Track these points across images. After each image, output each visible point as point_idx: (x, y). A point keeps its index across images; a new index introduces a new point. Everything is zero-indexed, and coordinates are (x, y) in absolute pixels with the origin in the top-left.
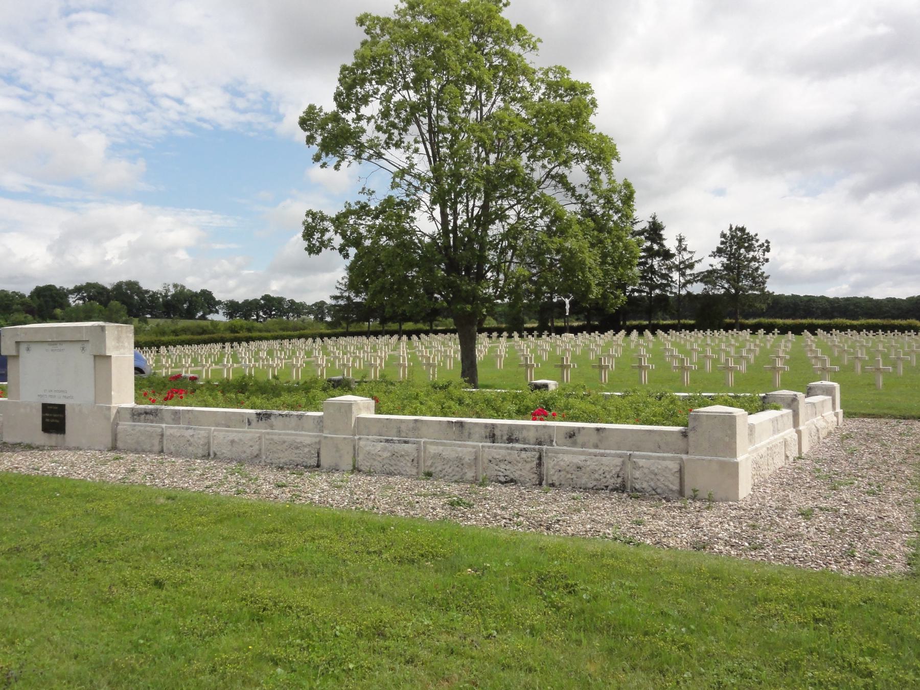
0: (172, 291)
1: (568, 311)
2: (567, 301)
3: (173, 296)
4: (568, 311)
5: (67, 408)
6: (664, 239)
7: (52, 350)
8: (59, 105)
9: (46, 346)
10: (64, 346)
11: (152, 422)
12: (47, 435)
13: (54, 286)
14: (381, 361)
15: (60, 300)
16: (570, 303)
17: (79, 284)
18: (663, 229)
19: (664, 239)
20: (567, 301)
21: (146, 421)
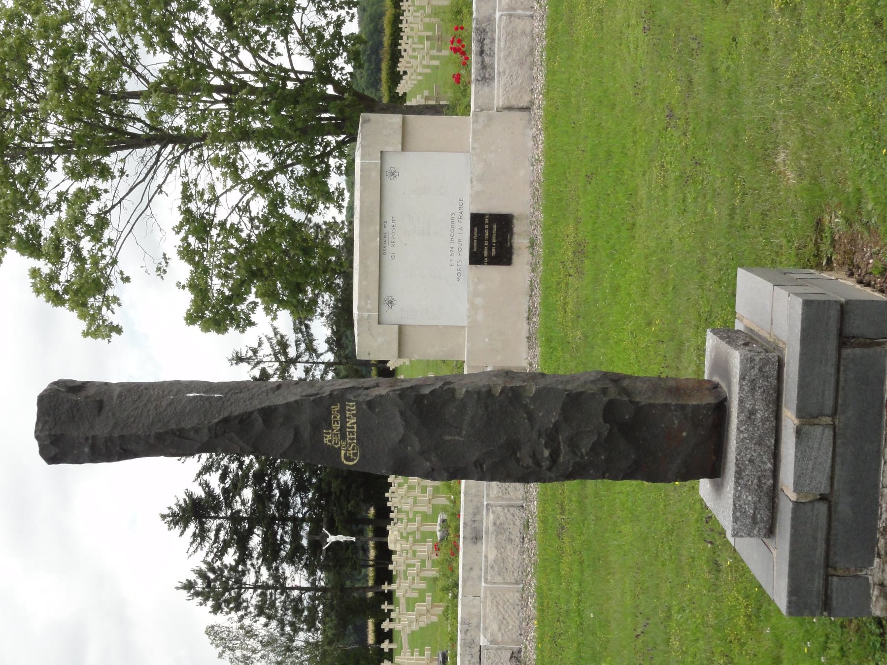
1: (349, 538)
2: (332, 539)
4: (349, 538)
5: (475, 212)
7: (393, 246)
9: (387, 258)
10: (388, 218)
11: (493, 40)
12: (515, 258)
16: (334, 533)
20: (332, 539)
21: (492, 56)
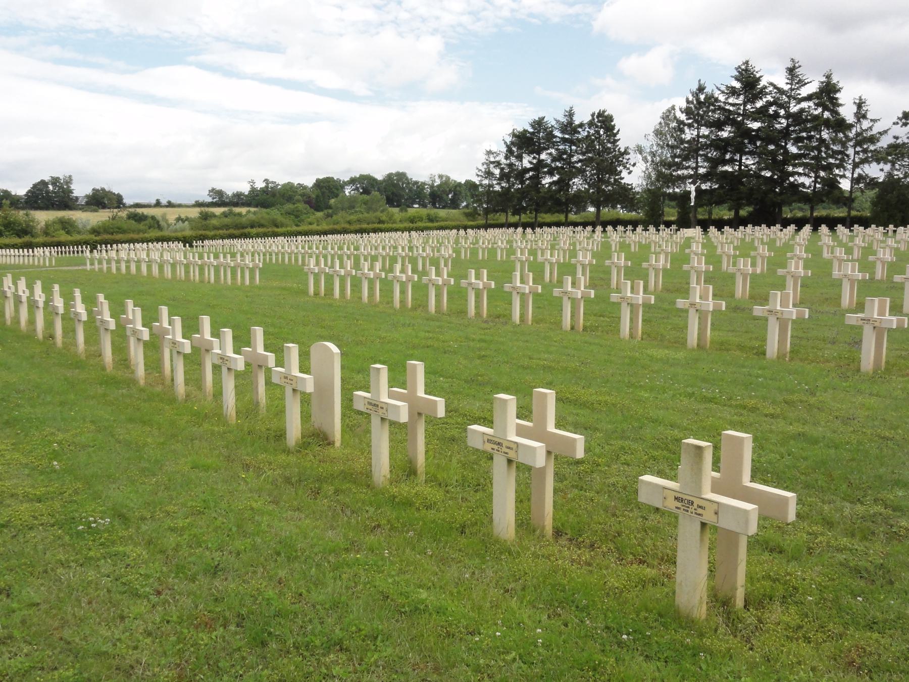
0: (438, 182)
3: (438, 186)
6: (841, 105)
8: (406, 11)
13: (333, 178)
14: (676, 246)
15: (336, 191)
17: (281, 179)
18: (839, 90)
19: (841, 105)
